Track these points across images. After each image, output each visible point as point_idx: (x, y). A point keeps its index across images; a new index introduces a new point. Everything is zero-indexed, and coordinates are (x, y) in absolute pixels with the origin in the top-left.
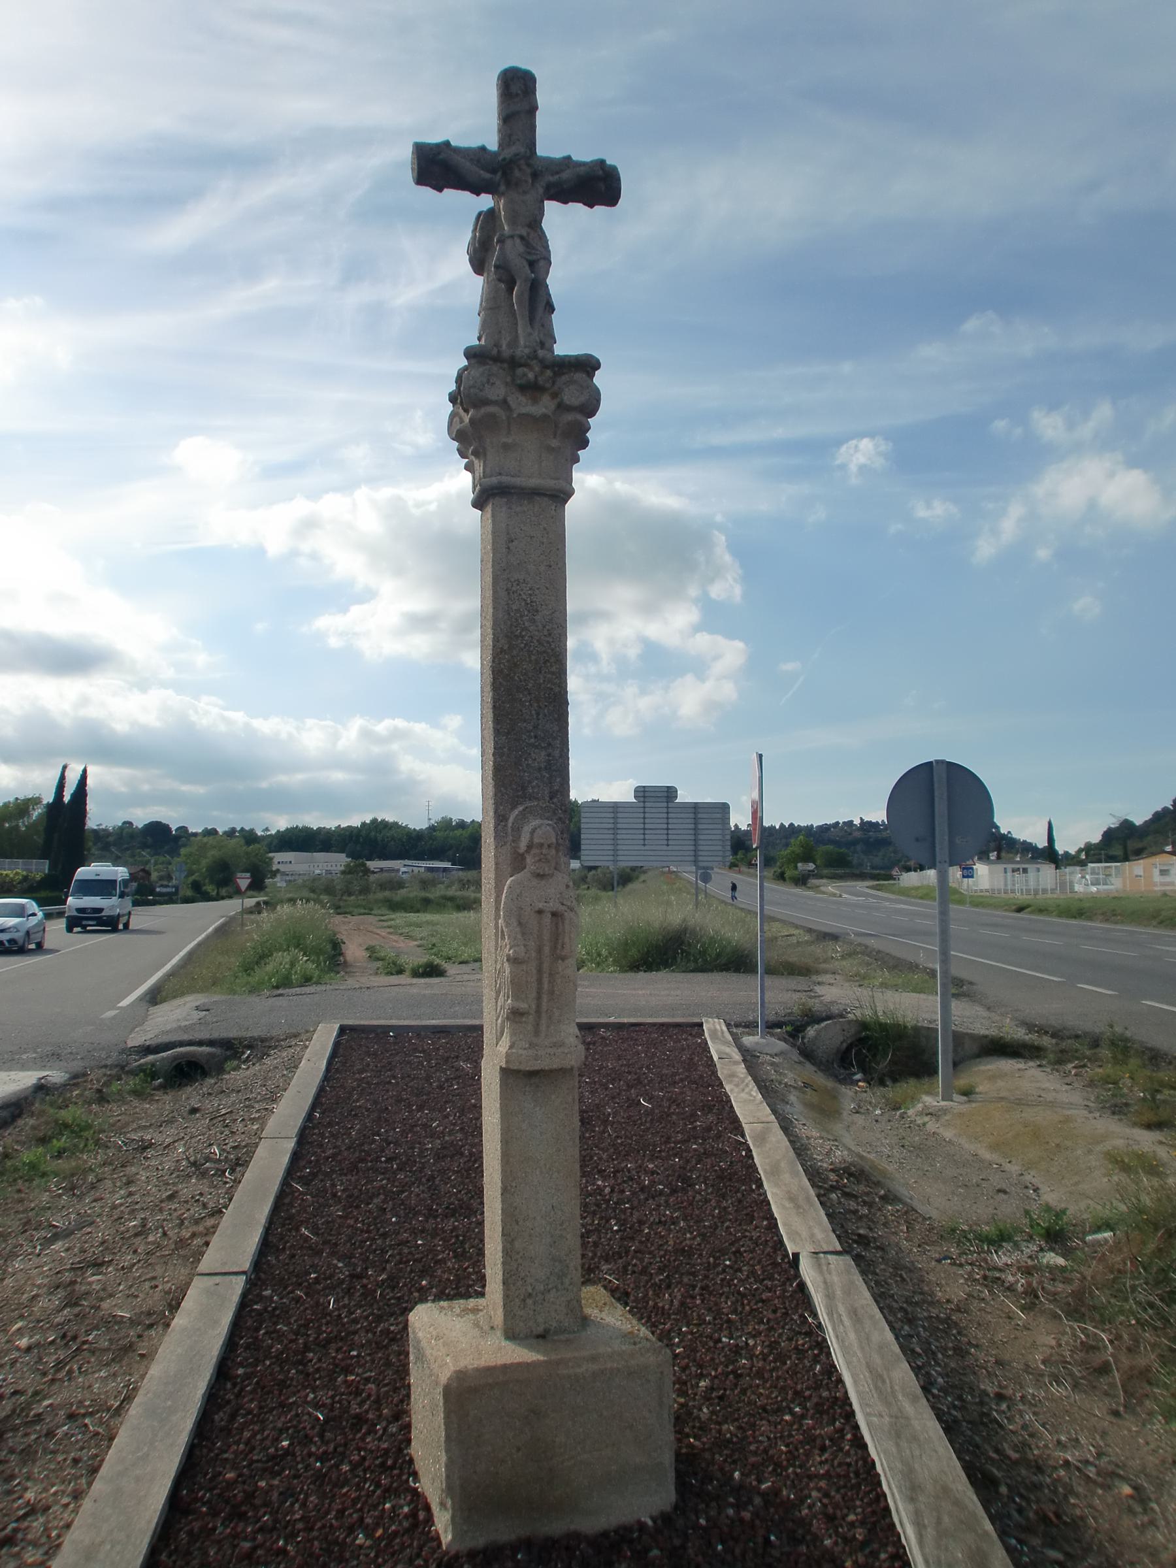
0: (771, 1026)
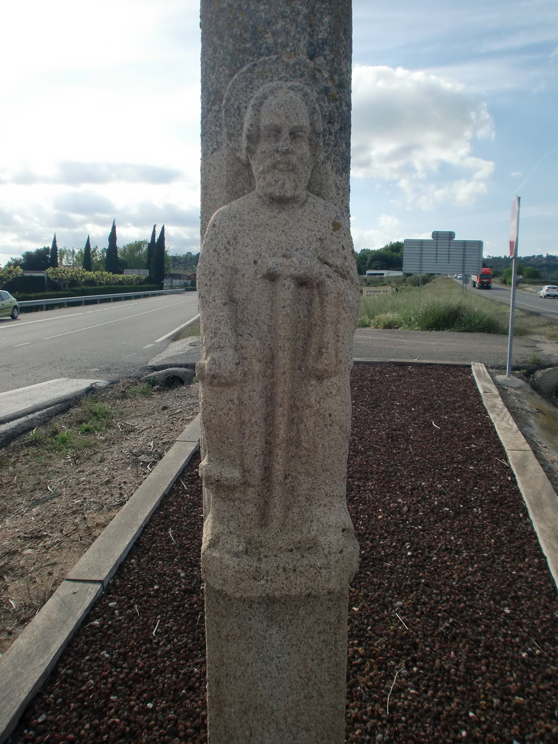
0: (514, 369)
